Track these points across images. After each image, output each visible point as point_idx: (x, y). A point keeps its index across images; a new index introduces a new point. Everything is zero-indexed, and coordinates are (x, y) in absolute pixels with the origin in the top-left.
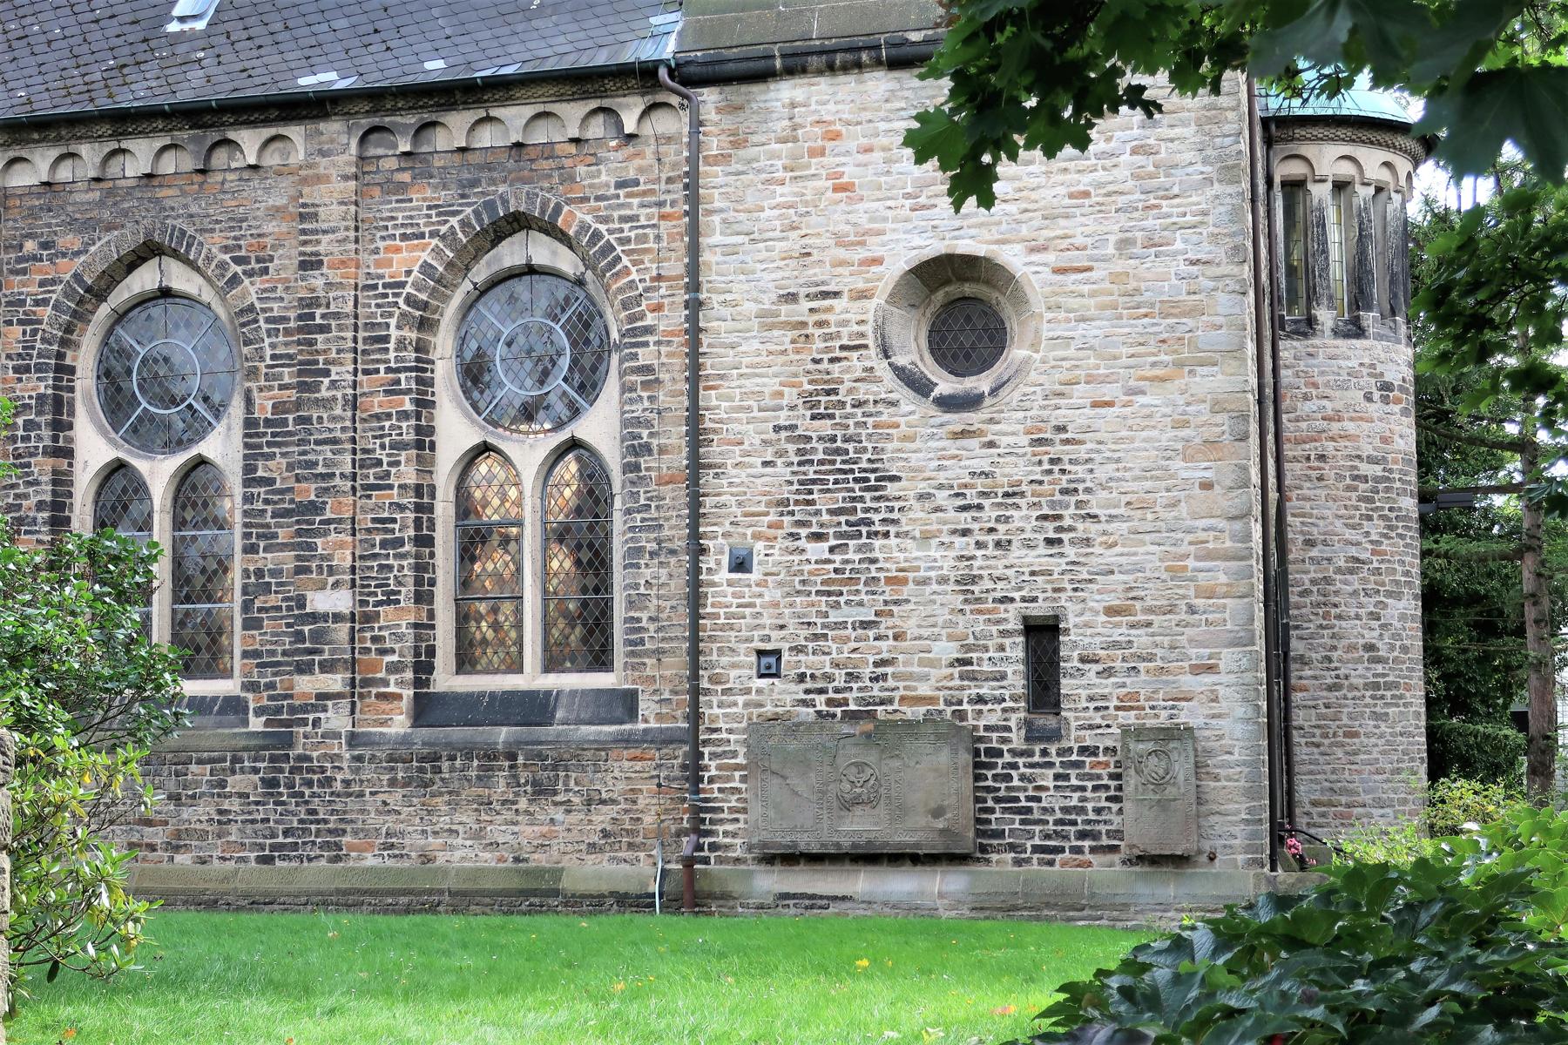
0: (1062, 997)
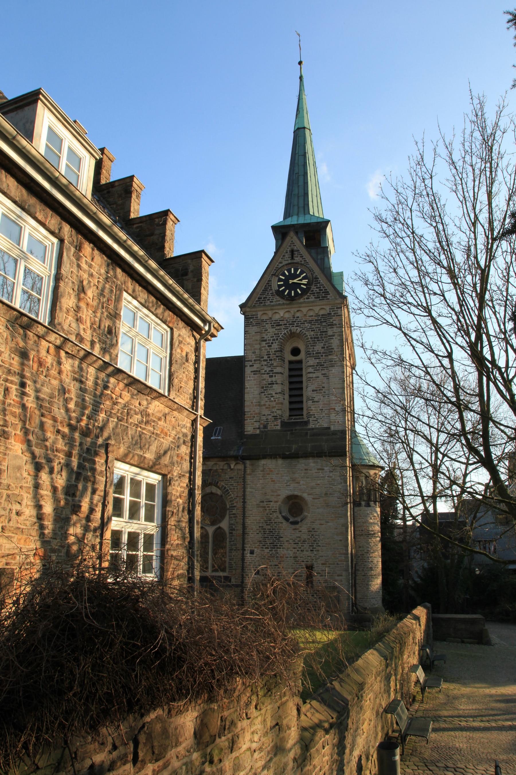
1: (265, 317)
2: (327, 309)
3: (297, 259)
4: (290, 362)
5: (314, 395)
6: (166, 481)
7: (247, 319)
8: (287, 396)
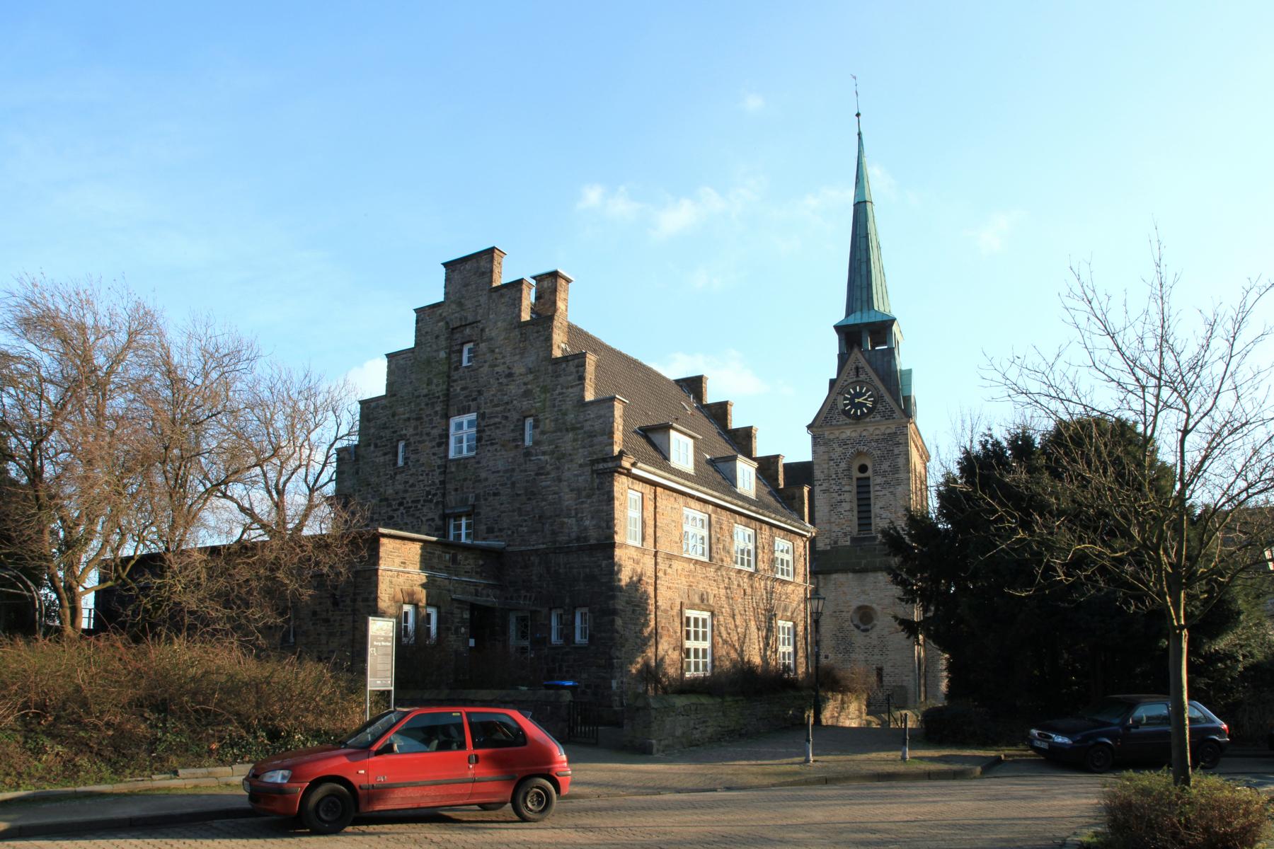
0: (560, 345)
1: (832, 437)
2: (893, 428)
3: (862, 377)
4: (858, 479)
5: (882, 512)
6: (795, 625)
7: (814, 438)
8: (855, 513)
